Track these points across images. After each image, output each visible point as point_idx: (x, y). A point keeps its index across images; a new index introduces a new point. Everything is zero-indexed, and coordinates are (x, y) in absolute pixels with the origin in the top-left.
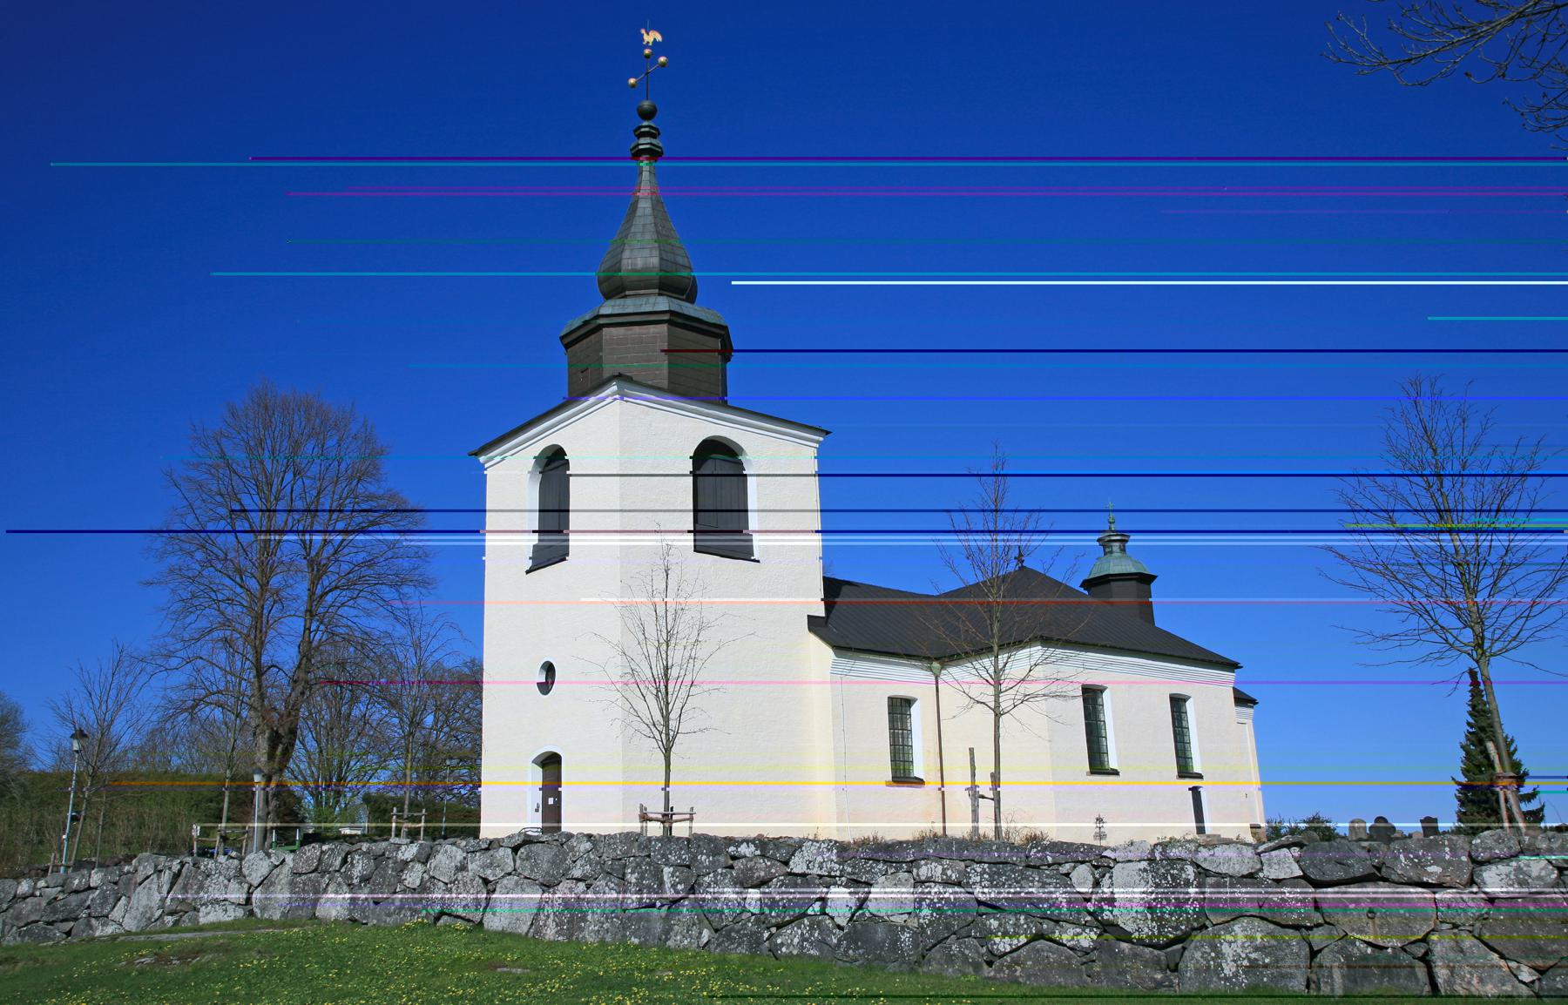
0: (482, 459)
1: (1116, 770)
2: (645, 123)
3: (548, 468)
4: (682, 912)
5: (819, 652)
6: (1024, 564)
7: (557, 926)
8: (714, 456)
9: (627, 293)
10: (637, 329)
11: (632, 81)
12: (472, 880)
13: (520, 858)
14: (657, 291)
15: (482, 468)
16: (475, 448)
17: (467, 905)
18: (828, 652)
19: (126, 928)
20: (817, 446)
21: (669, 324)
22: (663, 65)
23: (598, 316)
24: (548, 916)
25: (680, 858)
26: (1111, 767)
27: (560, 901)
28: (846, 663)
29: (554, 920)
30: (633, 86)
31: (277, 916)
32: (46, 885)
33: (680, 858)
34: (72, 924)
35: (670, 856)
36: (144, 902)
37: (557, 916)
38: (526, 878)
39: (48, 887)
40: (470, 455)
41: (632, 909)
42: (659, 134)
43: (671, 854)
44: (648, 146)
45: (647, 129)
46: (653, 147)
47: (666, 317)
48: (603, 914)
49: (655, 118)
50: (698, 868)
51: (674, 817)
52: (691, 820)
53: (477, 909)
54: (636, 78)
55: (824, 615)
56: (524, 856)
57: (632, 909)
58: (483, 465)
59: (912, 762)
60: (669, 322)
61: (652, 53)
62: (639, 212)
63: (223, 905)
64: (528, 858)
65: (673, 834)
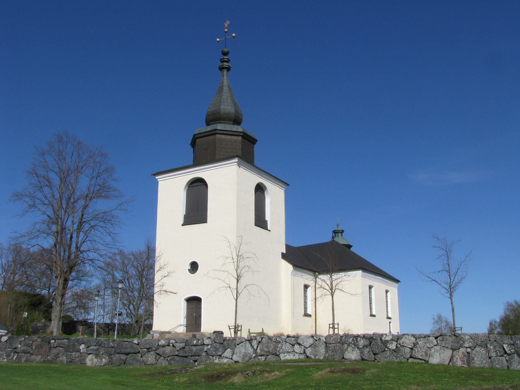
0: (157, 178)
1: (311, 315)
2: (225, 57)
3: (191, 186)
4: (515, 358)
5: (287, 267)
6: (334, 239)
7: (462, 361)
8: (259, 190)
9: (221, 121)
10: (229, 137)
11: (218, 40)
12: (423, 347)
13: (440, 340)
14: (232, 122)
15: (157, 183)
16: (155, 172)
17: (422, 355)
18: (290, 267)
19: (235, 360)
20: (284, 189)
21: (242, 137)
22: (234, 37)
23: (216, 130)
24: (457, 358)
25: (509, 342)
26: (373, 314)
27: (462, 354)
28: (296, 272)
29: (460, 360)
30: (218, 42)
31: (322, 358)
32: (175, 342)
33: (509, 342)
34: (197, 357)
35: (504, 341)
36: (243, 350)
37: (461, 359)
38: (443, 346)
39: (176, 343)
40: (152, 175)
41: (494, 357)
42: (229, 60)
43: (504, 340)
44: (227, 66)
45: (226, 60)
46: (229, 67)
47: (241, 134)
48: (482, 358)
49: (228, 56)
50: (517, 345)
51: (456, 329)
52: (461, 330)
53: (426, 356)
54: (220, 39)
55: (285, 253)
56: (441, 340)
57: (494, 357)
58: (157, 179)
59: (307, 308)
60: (243, 137)
61: (228, 31)
62: (224, 91)
63: (293, 353)
64: (442, 340)
65: (335, 333)
